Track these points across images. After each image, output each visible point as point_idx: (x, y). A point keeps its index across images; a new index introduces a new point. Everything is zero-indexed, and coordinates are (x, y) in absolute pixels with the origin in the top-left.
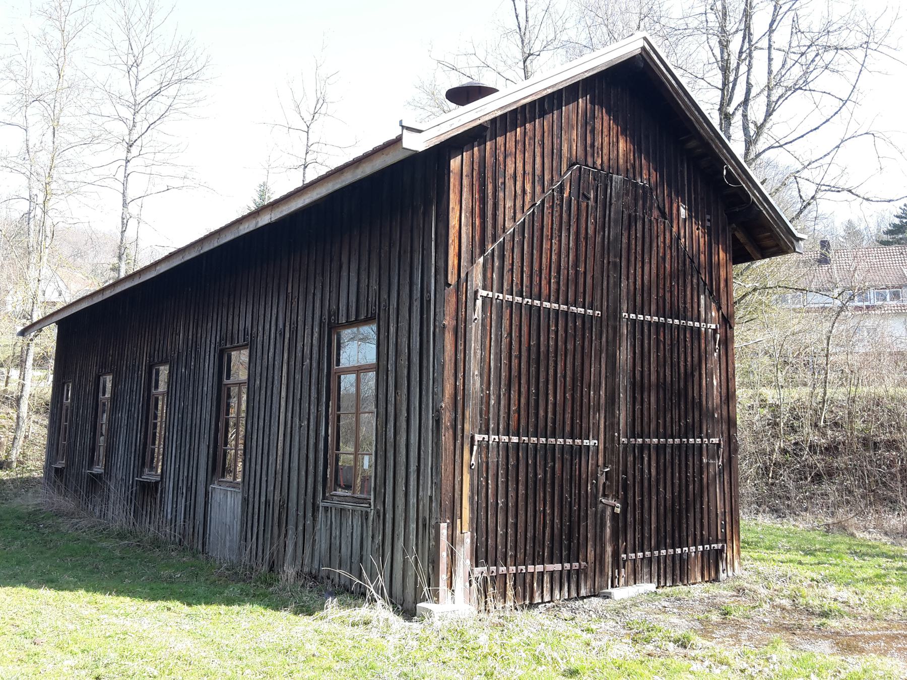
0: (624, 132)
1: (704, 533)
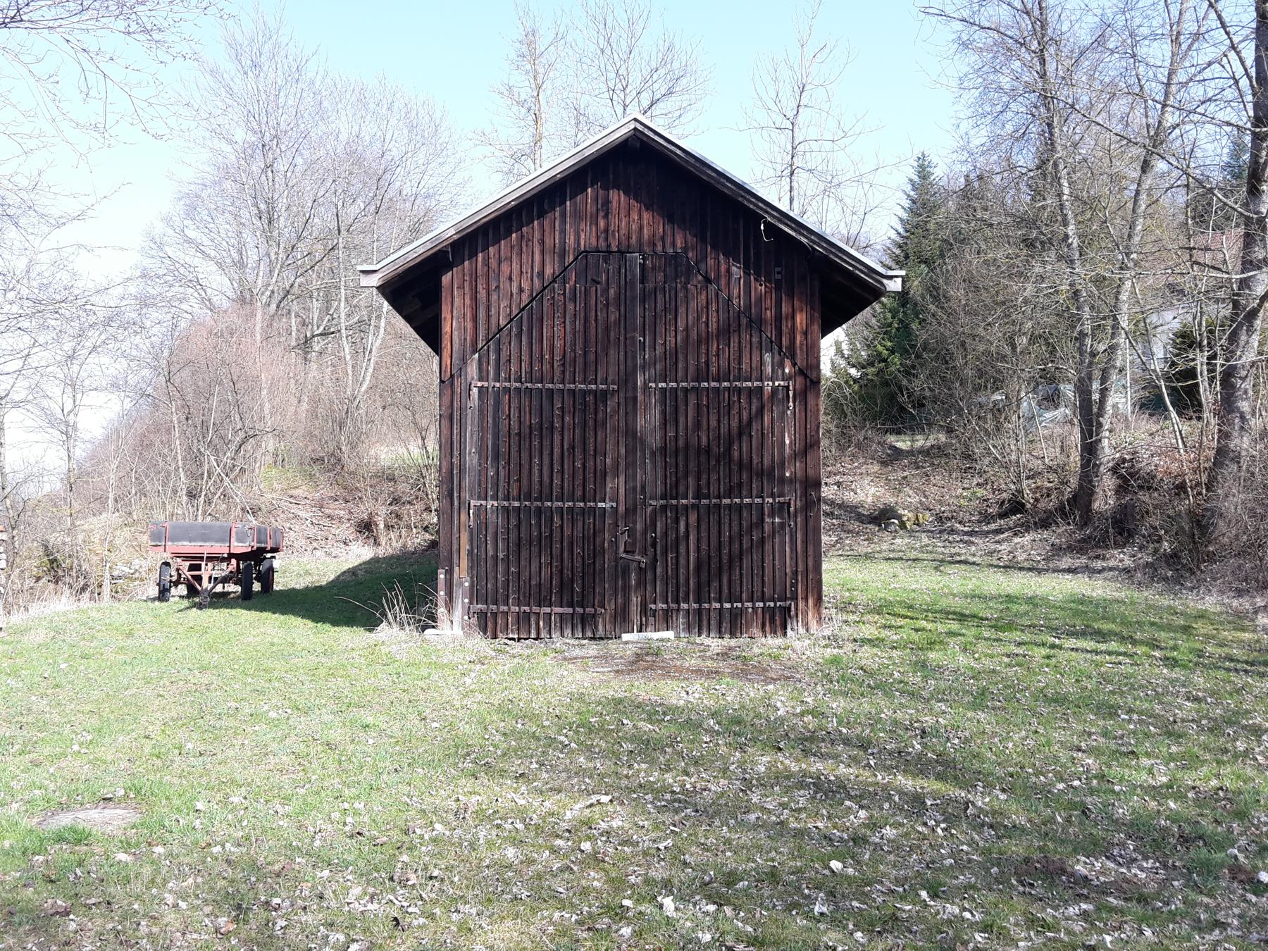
0: (648, 208)
1: (765, 590)
